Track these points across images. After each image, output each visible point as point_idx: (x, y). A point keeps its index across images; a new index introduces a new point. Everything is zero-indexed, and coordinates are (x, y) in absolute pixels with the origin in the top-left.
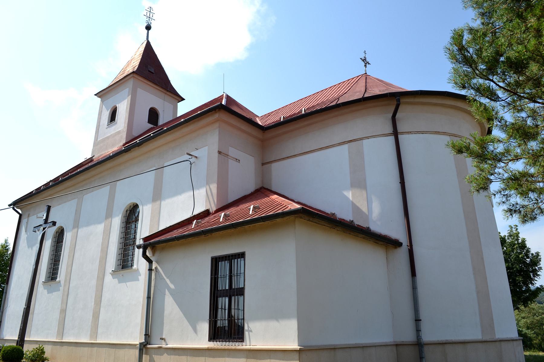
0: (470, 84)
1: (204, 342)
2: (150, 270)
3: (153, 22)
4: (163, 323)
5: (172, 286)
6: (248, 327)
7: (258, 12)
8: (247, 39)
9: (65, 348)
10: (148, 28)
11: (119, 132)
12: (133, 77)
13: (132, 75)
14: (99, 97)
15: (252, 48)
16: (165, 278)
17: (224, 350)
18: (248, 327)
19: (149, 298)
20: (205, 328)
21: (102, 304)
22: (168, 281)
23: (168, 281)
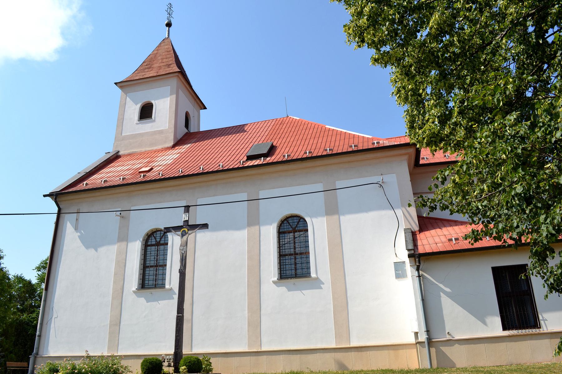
0: (463, 145)
1: (499, 331)
2: (419, 276)
3: (172, 19)
4: (478, 319)
5: (448, 290)
6: (543, 317)
7: (74, 17)
8: (57, 42)
9: (264, 358)
10: (169, 25)
11: (161, 132)
12: (178, 76)
13: (177, 74)
14: (121, 87)
15: (62, 51)
16: (437, 283)
17: (531, 335)
18: (543, 317)
19: (423, 300)
20: (497, 321)
21: (262, 312)
22: (441, 286)
23: (441, 286)
